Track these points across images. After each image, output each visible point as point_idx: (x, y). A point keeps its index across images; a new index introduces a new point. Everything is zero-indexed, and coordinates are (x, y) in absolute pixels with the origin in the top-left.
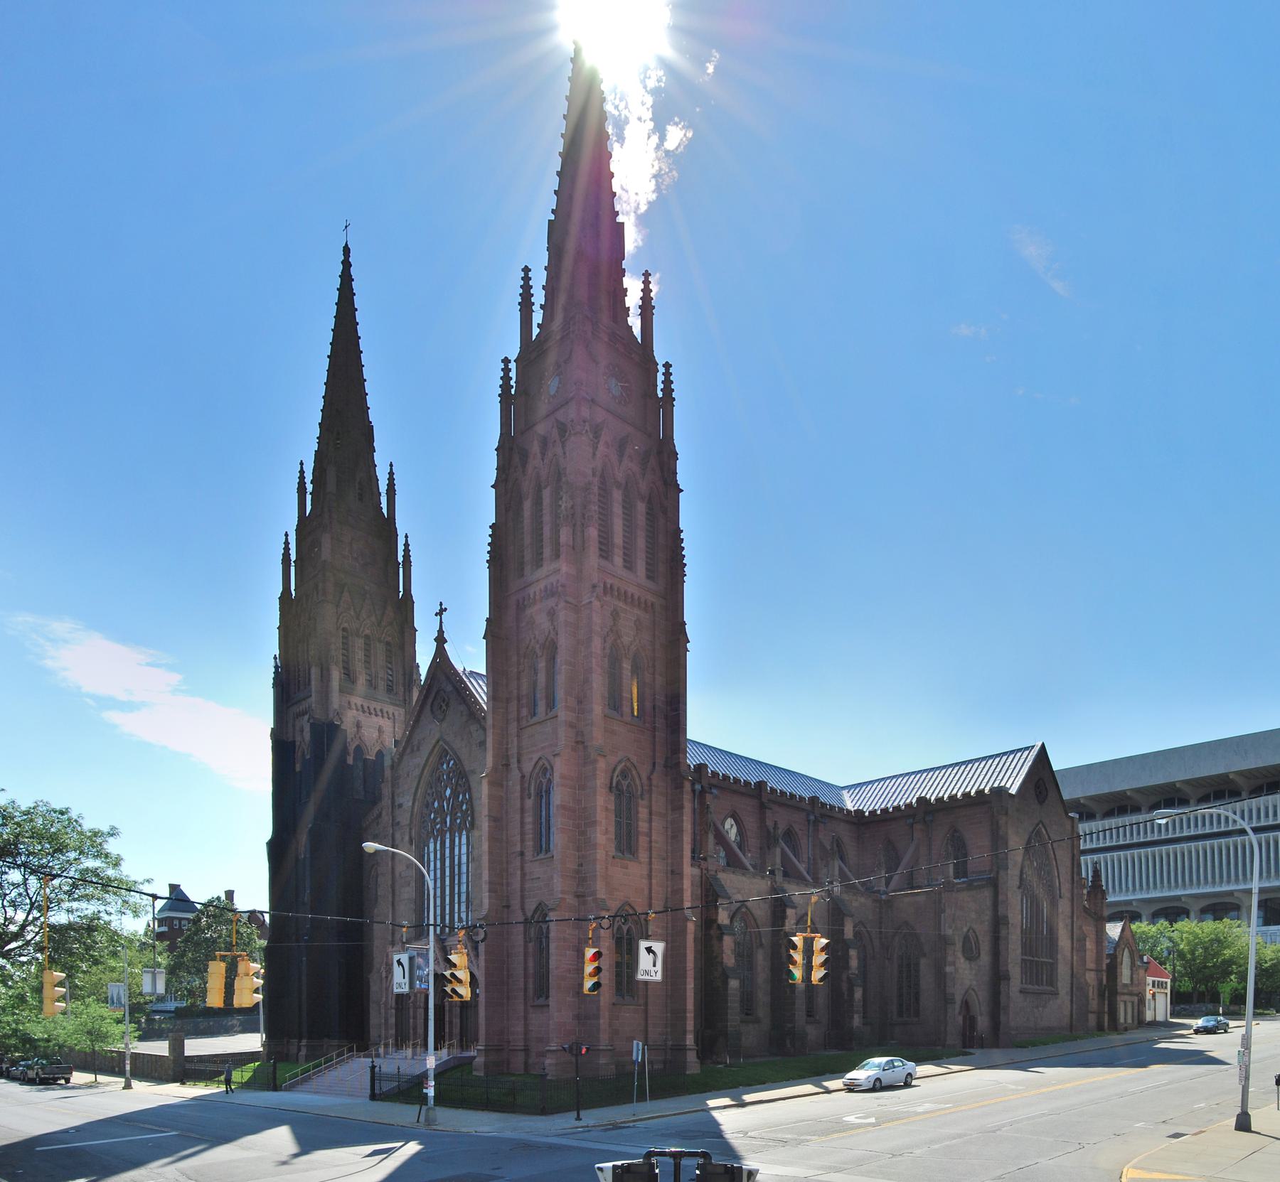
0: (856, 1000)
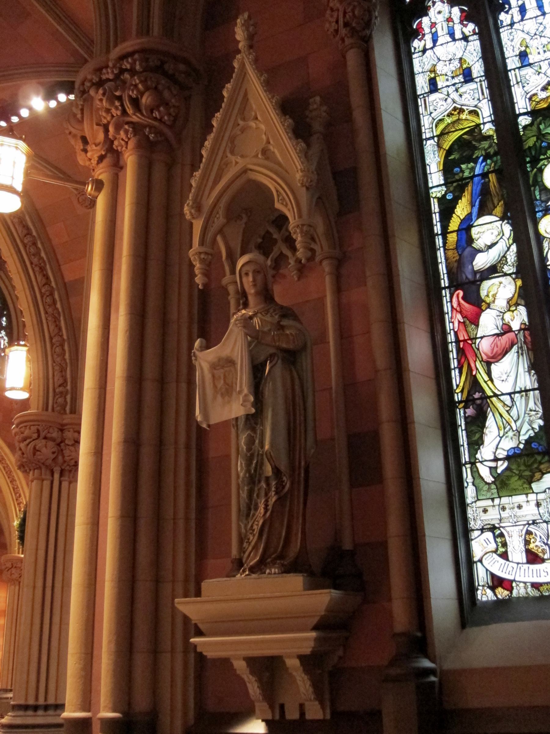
0: (510, 488)
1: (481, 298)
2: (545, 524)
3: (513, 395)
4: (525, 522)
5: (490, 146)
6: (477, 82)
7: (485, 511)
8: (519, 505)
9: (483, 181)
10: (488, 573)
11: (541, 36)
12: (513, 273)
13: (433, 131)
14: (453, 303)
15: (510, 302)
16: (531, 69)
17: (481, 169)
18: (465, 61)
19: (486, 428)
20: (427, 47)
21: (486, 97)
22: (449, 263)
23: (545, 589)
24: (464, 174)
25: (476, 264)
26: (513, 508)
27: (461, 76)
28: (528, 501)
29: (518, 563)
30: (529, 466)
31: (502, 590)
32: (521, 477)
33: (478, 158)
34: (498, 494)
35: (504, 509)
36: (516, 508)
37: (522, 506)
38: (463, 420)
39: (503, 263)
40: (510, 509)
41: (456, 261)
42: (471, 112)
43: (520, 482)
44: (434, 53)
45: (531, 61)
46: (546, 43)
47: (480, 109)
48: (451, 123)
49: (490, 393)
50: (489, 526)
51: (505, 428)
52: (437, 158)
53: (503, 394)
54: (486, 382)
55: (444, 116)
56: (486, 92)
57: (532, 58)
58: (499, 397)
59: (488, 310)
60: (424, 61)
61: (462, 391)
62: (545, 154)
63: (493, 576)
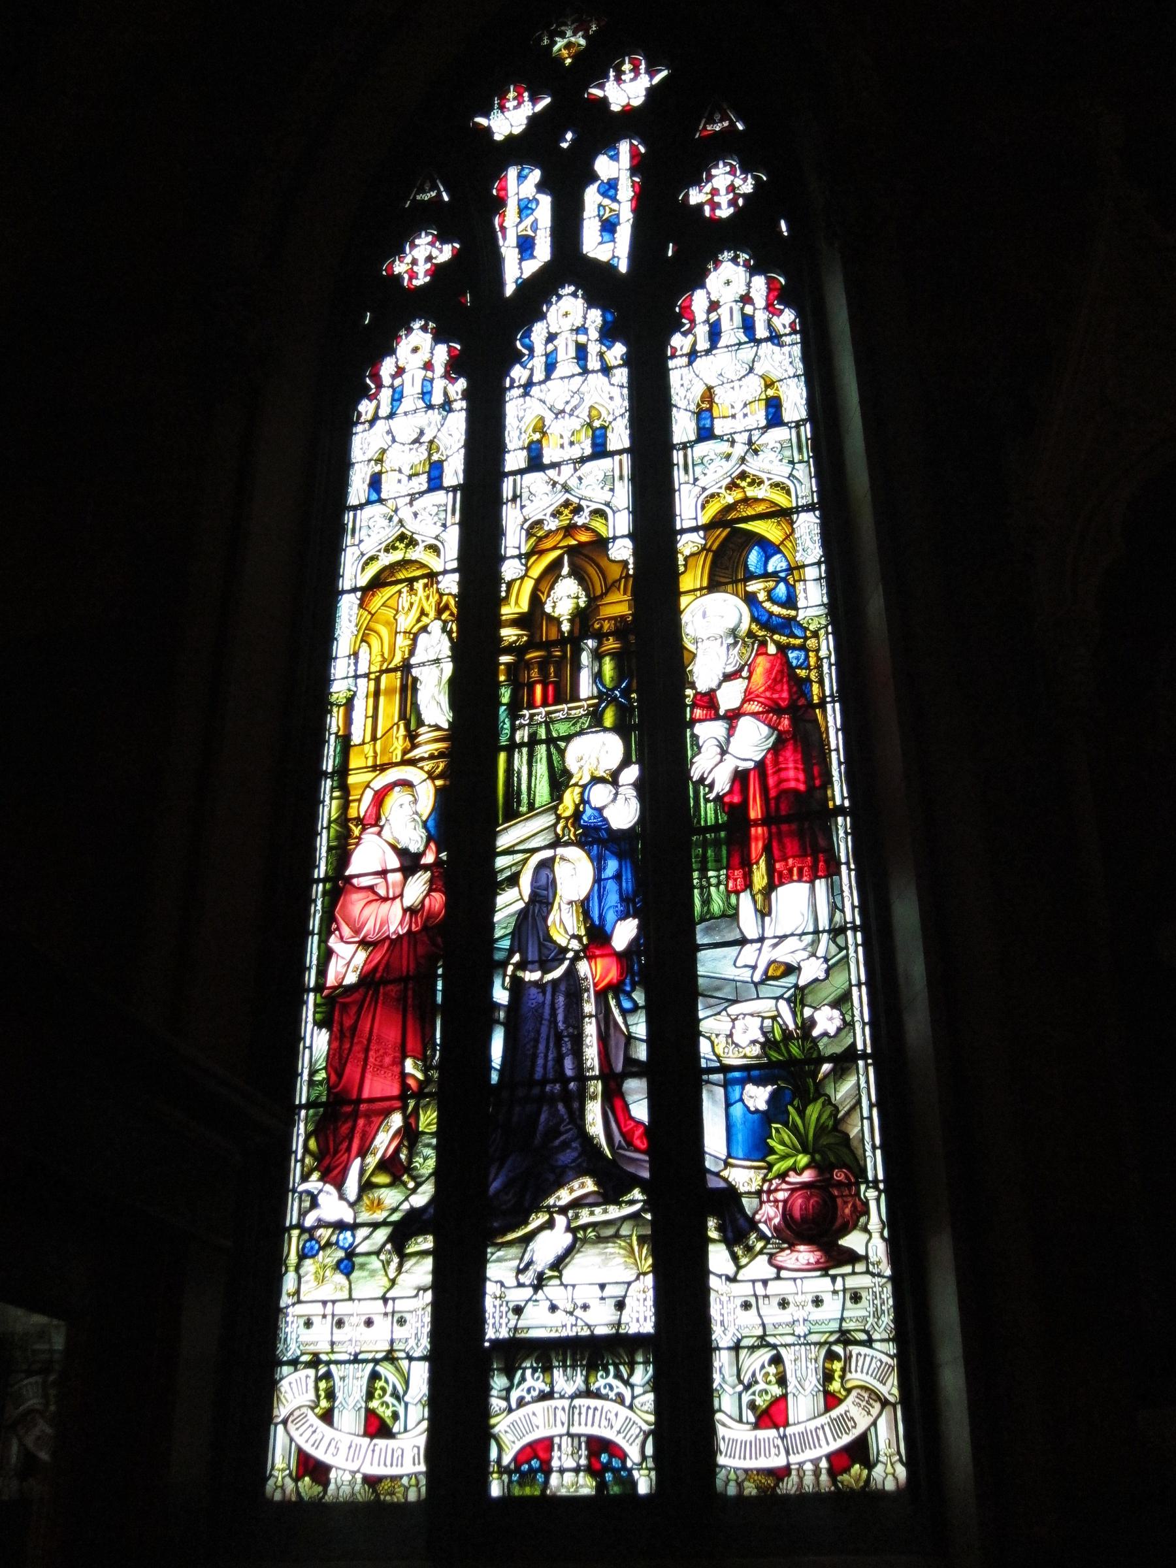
8: (817, 1297)
20: (535, 380)
63: (301, 1453)
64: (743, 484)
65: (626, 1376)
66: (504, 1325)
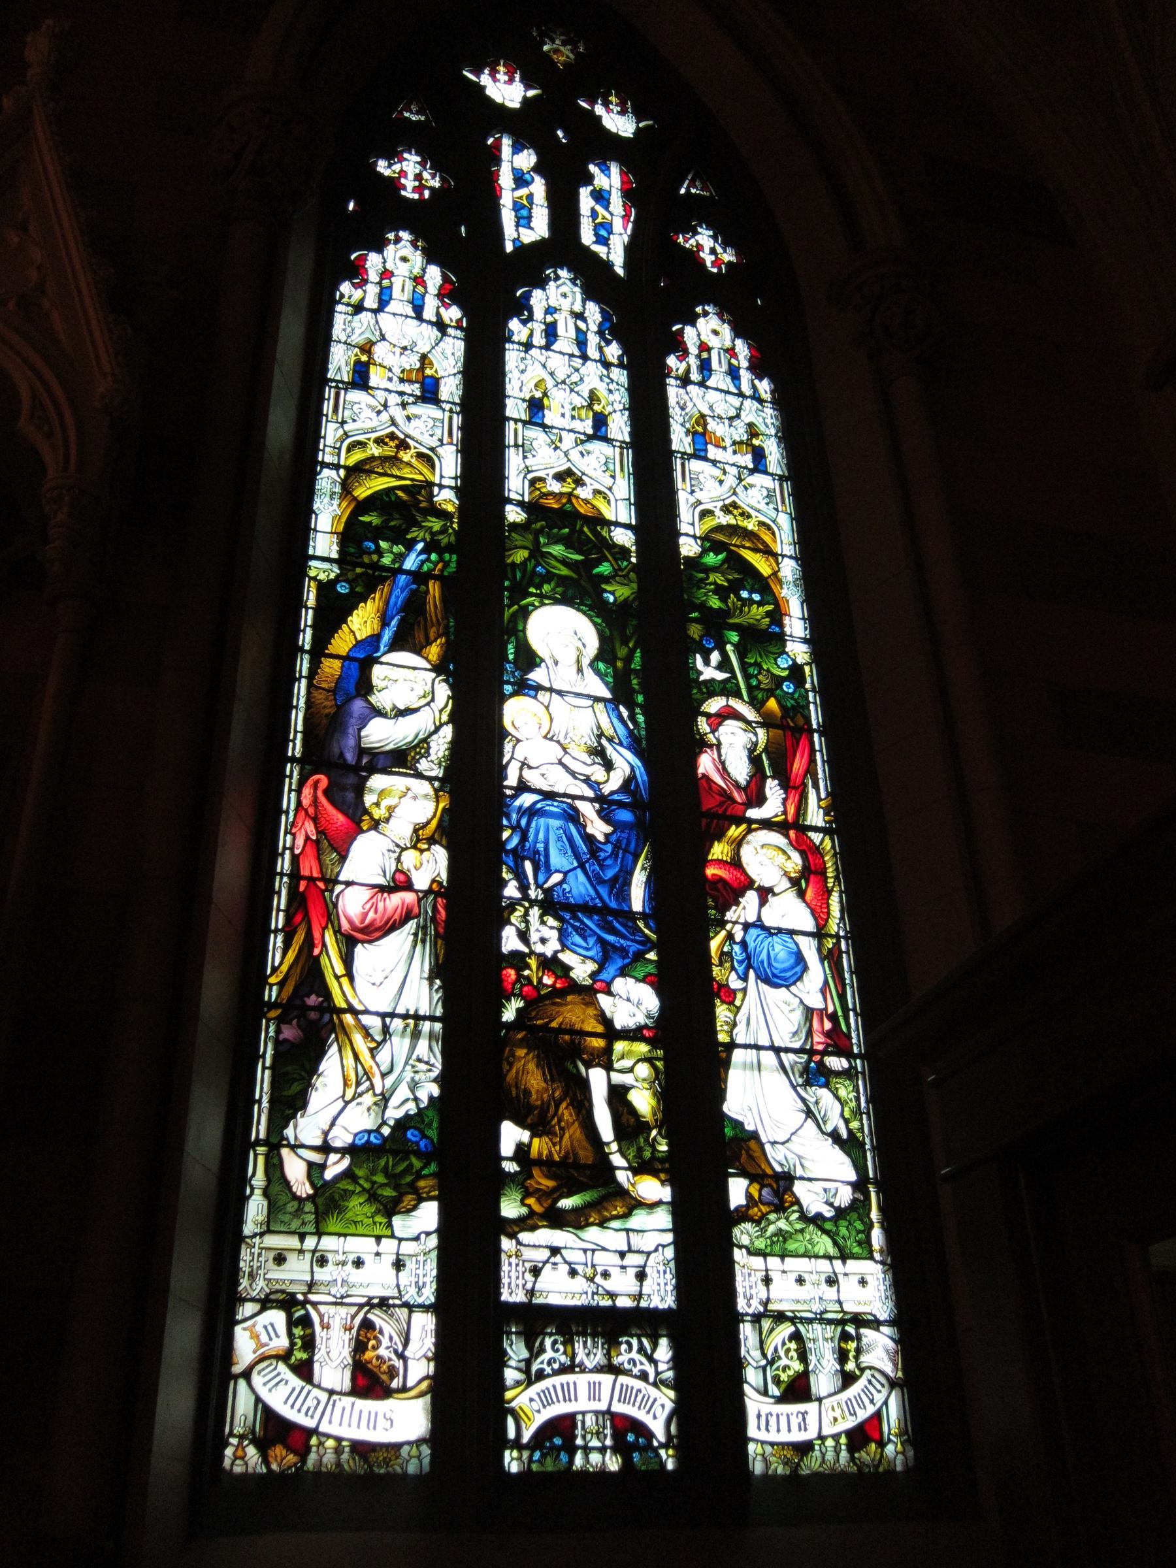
1: (363, 803)
2: (406, 1310)
3: (388, 1020)
4: (363, 1300)
5: (443, 531)
6: (444, 410)
7: (280, 1259)
8: (359, 1258)
9: (414, 586)
10: (260, 1406)
11: (572, 390)
12: (436, 778)
13: (339, 455)
14: (303, 795)
15: (421, 832)
16: (543, 434)
17: (416, 565)
18: (431, 363)
19: (319, 1076)
20: (367, 304)
21: (455, 442)
22: (312, 715)
23: (381, 1458)
24: (382, 560)
25: (367, 736)
26: (344, 1263)
27: (417, 385)
28: (378, 1254)
29: (331, 1392)
30: (394, 1179)
31: (284, 1452)
32: (373, 1197)
33: (414, 541)
34: (317, 1227)
35: (322, 1261)
36: (350, 1264)
37: (363, 1263)
38: (270, 1046)
39: (420, 753)
40: (337, 1265)
41: (327, 715)
42: (420, 455)
43: (369, 1209)
44: (377, 322)
45: (547, 421)
46: (579, 406)
47: (439, 458)
48: (380, 457)
49: (340, 1003)
50: (281, 1297)
51: (358, 1084)
52: (335, 507)
53: (366, 1012)
54: (337, 978)
55: (369, 439)
56: (457, 435)
57: (550, 418)
58: (360, 1016)
59: (373, 833)
60: (353, 324)
61: (281, 984)
62: (539, 587)
64: (735, 512)
65: (649, 1352)
66: (521, 1286)
